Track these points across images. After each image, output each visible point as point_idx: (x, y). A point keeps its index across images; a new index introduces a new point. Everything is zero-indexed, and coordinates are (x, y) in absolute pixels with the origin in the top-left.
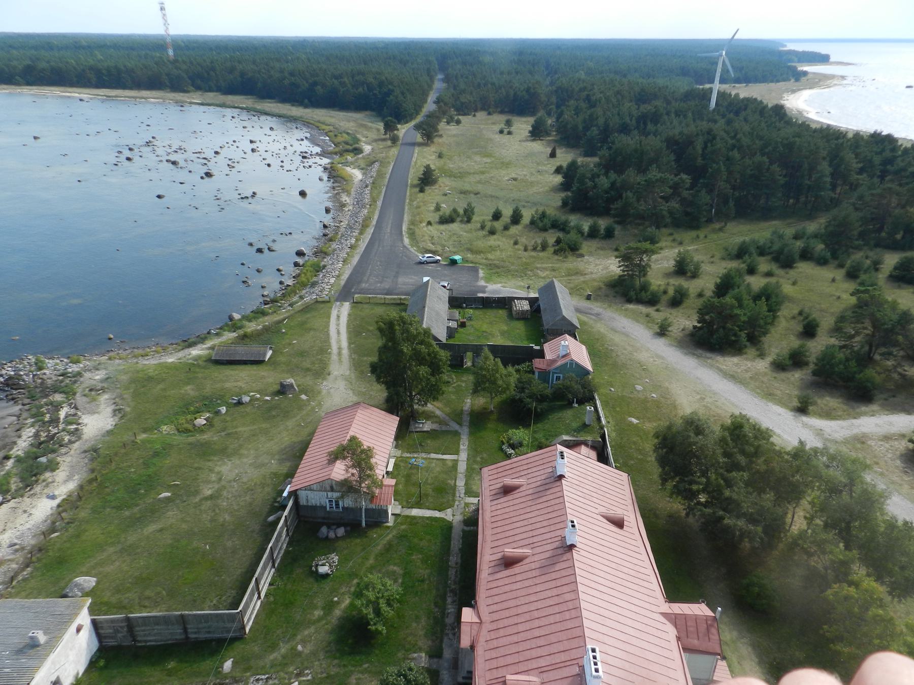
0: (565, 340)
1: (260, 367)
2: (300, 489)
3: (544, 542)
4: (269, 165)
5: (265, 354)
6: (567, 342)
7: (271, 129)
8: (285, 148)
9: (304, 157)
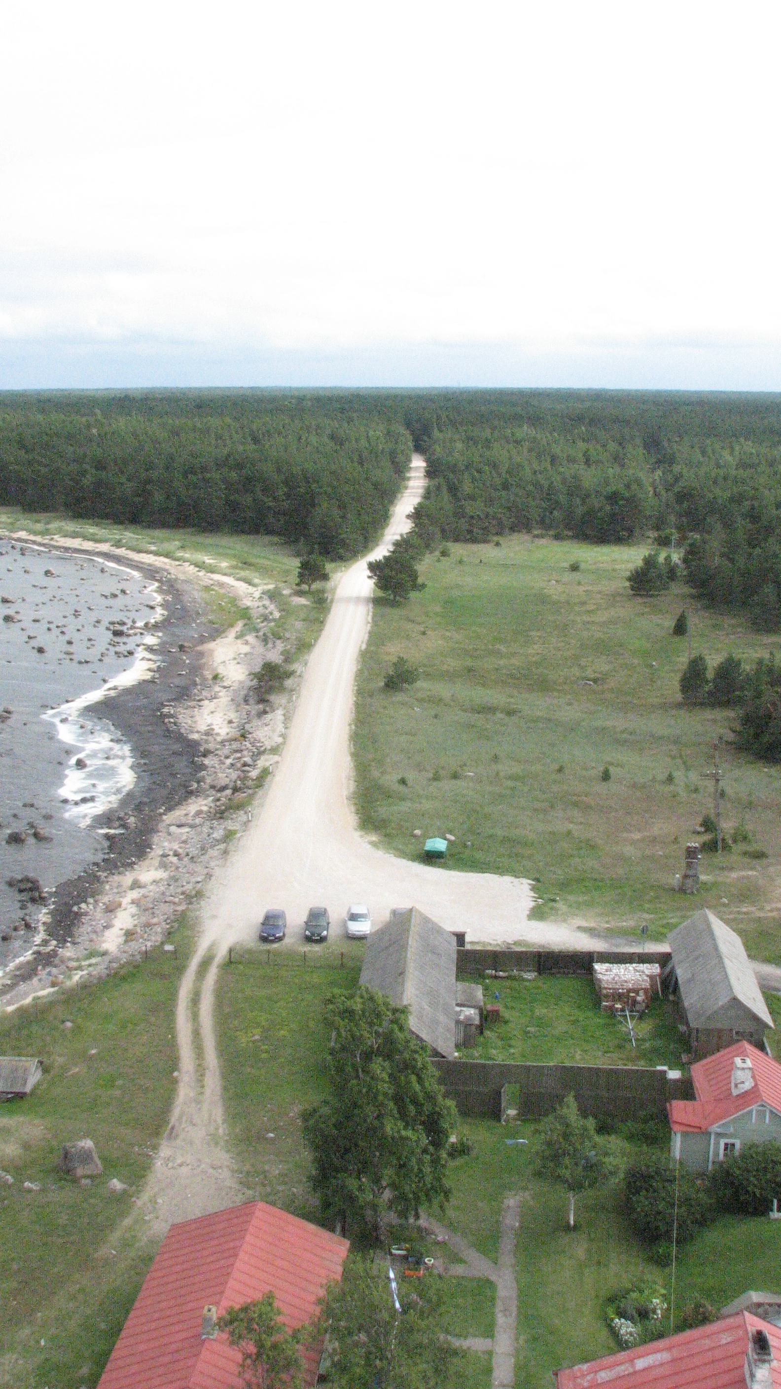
4: (41, 650)
7: (48, 573)
8: (76, 614)
9: (117, 633)
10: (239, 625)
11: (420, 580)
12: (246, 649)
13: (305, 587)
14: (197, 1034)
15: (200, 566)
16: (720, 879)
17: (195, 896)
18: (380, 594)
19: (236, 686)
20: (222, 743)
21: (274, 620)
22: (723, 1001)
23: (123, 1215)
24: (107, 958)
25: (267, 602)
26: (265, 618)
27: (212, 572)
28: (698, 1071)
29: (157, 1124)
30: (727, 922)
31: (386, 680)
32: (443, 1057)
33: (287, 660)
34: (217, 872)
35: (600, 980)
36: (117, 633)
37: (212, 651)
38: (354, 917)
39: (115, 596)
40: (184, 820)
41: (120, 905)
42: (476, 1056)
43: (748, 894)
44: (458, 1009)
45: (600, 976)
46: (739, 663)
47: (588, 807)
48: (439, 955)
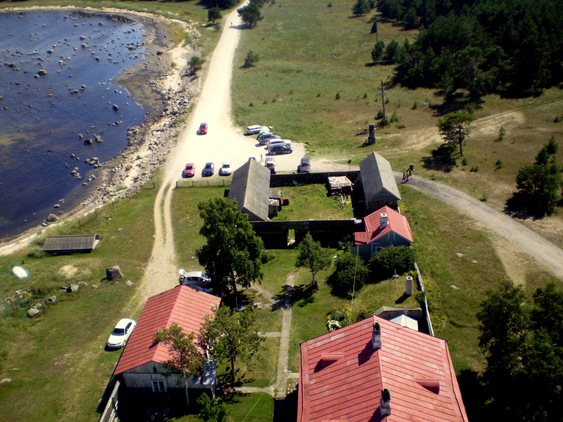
0: (385, 211)
1: (238, 403)
2: (125, 372)
3: (360, 412)
5: (91, 243)
6: (387, 213)
10: (183, 42)
11: (261, 16)
12: (186, 51)
13: (211, 22)
14: (163, 218)
15: (166, 16)
16: (384, 138)
17: (162, 161)
18: (244, 23)
19: (181, 68)
20: (175, 94)
21: (198, 38)
22: (379, 190)
23: (132, 294)
24: (126, 190)
25: (195, 30)
26: (195, 38)
27: (171, 18)
28: (366, 219)
29: (146, 257)
30: (385, 157)
31: (247, 62)
32: (262, 220)
33: (203, 56)
34: (172, 150)
35: (330, 184)
36: (130, 49)
37: (171, 54)
38: (226, 166)
39: (129, 32)
40: (159, 129)
41: (132, 167)
42: (275, 219)
43: (396, 143)
44: (270, 200)
45: (330, 182)
46: (397, 44)
47: (330, 110)
48: (263, 178)
